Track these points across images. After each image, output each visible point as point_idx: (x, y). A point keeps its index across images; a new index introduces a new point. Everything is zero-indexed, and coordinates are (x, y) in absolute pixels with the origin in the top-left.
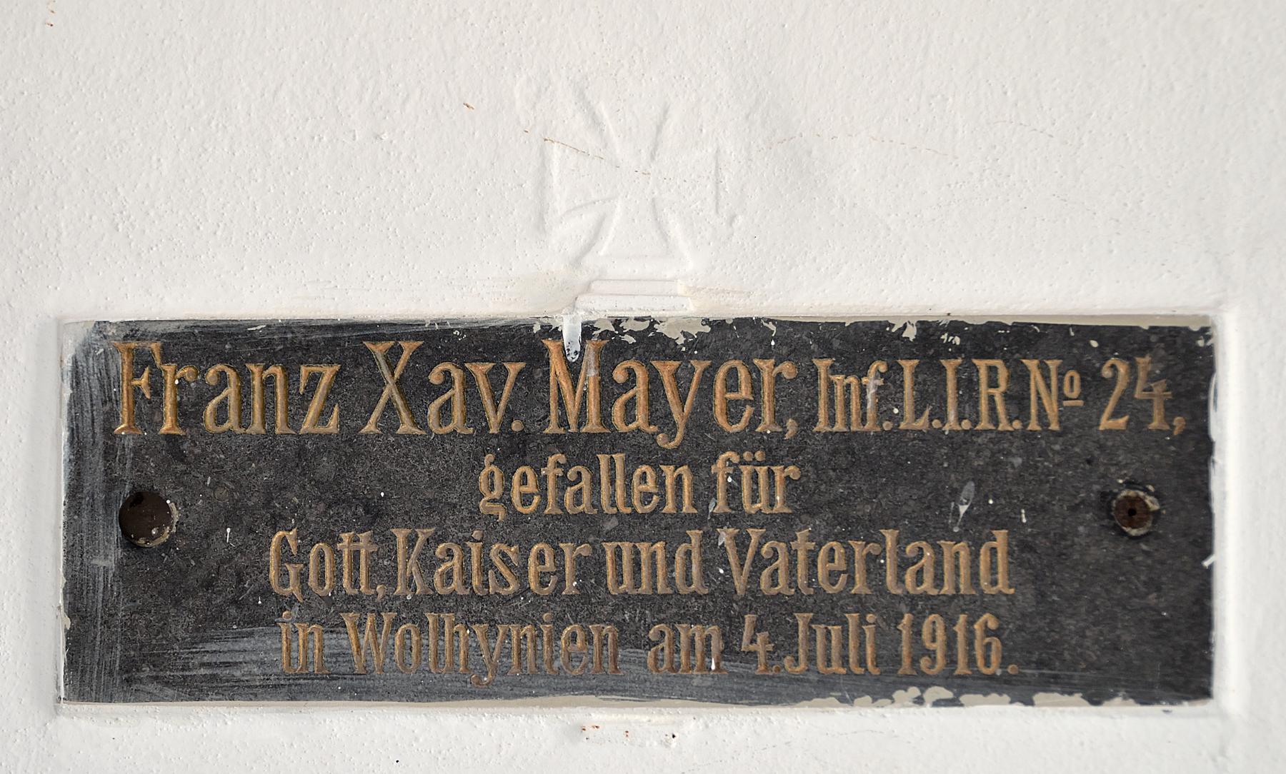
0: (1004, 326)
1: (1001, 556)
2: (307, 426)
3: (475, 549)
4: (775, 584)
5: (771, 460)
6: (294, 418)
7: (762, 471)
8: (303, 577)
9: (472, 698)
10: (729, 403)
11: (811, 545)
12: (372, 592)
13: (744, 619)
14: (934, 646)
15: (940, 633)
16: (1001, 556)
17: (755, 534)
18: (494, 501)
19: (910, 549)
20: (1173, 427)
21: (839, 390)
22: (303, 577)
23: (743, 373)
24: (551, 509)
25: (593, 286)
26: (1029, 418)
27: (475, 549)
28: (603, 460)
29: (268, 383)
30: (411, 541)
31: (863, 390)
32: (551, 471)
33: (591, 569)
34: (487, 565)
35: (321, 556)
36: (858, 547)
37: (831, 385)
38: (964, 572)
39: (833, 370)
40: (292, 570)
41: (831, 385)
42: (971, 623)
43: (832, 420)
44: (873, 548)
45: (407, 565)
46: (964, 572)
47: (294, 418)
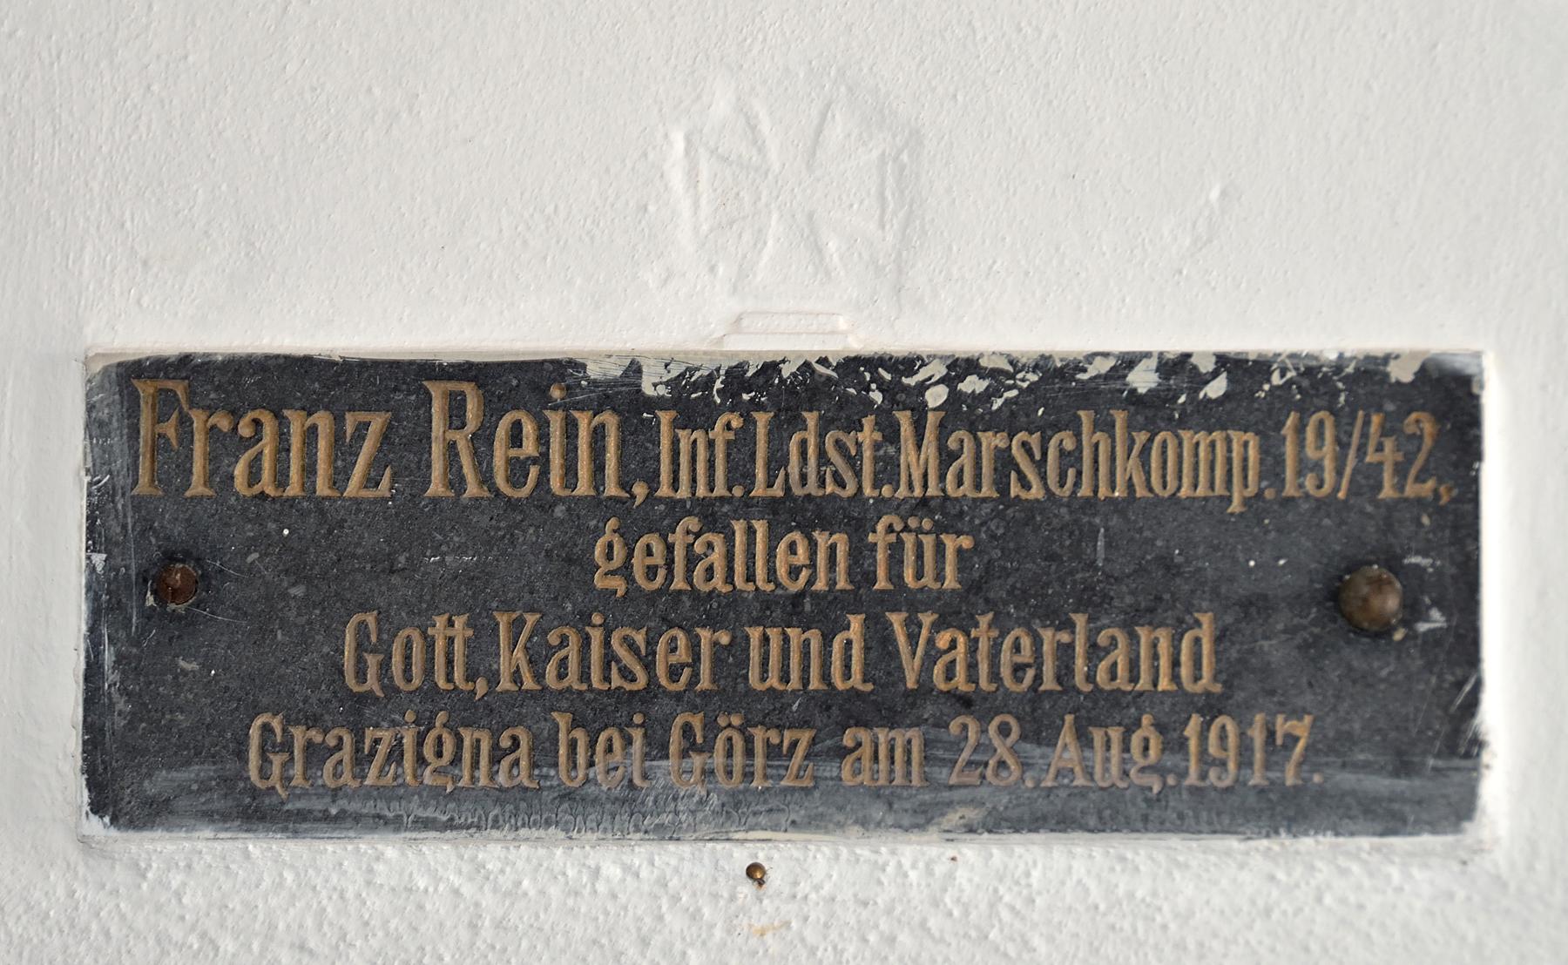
0: (335, 363)
1: (856, 652)
2: (353, 488)
3: (596, 636)
4: (1113, 677)
5: (939, 529)
6: (340, 477)
7: (928, 541)
8: (385, 666)
9: (373, 829)
10: (512, 463)
11: (995, 633)
12: (470, 686)
13: (1063, 720)
14: (270, 783)
15: (1232, 740)
16: (856, 652)
17: (927, 619)
18: (612, 573)
19: (943, 640)
20: (633, 497)
21: (684, 446)
22: (385, 666)
23: (529, 428)
24: (820, 585)
25: (745, 323)
26: (753, 483)
27: (596, 636)
28: (739, 527)
29: (311, 434)
30: (517, 625)
31: (711, 444)
32: (678, 538)
33: (731, 660)
34: (609, 658)
35: (408, 645)
36: (1047, 635)
37: (675, 442)
38: (1164, 663)
39: (675, 425)
40: (372, 661)
41: (675, 442)
42: (1205, 728)
43: (675, 484)
44: (1065, 637)
45: (510, 660)
46: (1164, 663)
47: (340, 477)
